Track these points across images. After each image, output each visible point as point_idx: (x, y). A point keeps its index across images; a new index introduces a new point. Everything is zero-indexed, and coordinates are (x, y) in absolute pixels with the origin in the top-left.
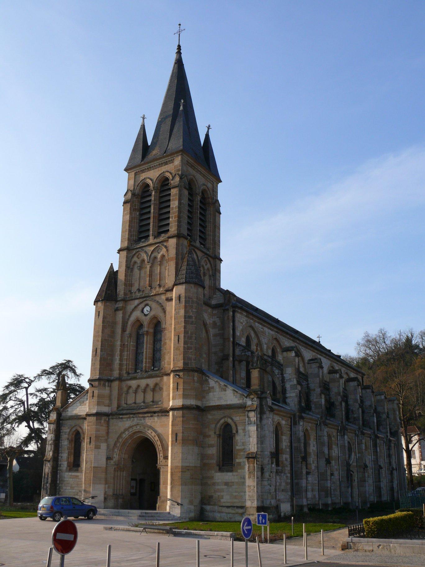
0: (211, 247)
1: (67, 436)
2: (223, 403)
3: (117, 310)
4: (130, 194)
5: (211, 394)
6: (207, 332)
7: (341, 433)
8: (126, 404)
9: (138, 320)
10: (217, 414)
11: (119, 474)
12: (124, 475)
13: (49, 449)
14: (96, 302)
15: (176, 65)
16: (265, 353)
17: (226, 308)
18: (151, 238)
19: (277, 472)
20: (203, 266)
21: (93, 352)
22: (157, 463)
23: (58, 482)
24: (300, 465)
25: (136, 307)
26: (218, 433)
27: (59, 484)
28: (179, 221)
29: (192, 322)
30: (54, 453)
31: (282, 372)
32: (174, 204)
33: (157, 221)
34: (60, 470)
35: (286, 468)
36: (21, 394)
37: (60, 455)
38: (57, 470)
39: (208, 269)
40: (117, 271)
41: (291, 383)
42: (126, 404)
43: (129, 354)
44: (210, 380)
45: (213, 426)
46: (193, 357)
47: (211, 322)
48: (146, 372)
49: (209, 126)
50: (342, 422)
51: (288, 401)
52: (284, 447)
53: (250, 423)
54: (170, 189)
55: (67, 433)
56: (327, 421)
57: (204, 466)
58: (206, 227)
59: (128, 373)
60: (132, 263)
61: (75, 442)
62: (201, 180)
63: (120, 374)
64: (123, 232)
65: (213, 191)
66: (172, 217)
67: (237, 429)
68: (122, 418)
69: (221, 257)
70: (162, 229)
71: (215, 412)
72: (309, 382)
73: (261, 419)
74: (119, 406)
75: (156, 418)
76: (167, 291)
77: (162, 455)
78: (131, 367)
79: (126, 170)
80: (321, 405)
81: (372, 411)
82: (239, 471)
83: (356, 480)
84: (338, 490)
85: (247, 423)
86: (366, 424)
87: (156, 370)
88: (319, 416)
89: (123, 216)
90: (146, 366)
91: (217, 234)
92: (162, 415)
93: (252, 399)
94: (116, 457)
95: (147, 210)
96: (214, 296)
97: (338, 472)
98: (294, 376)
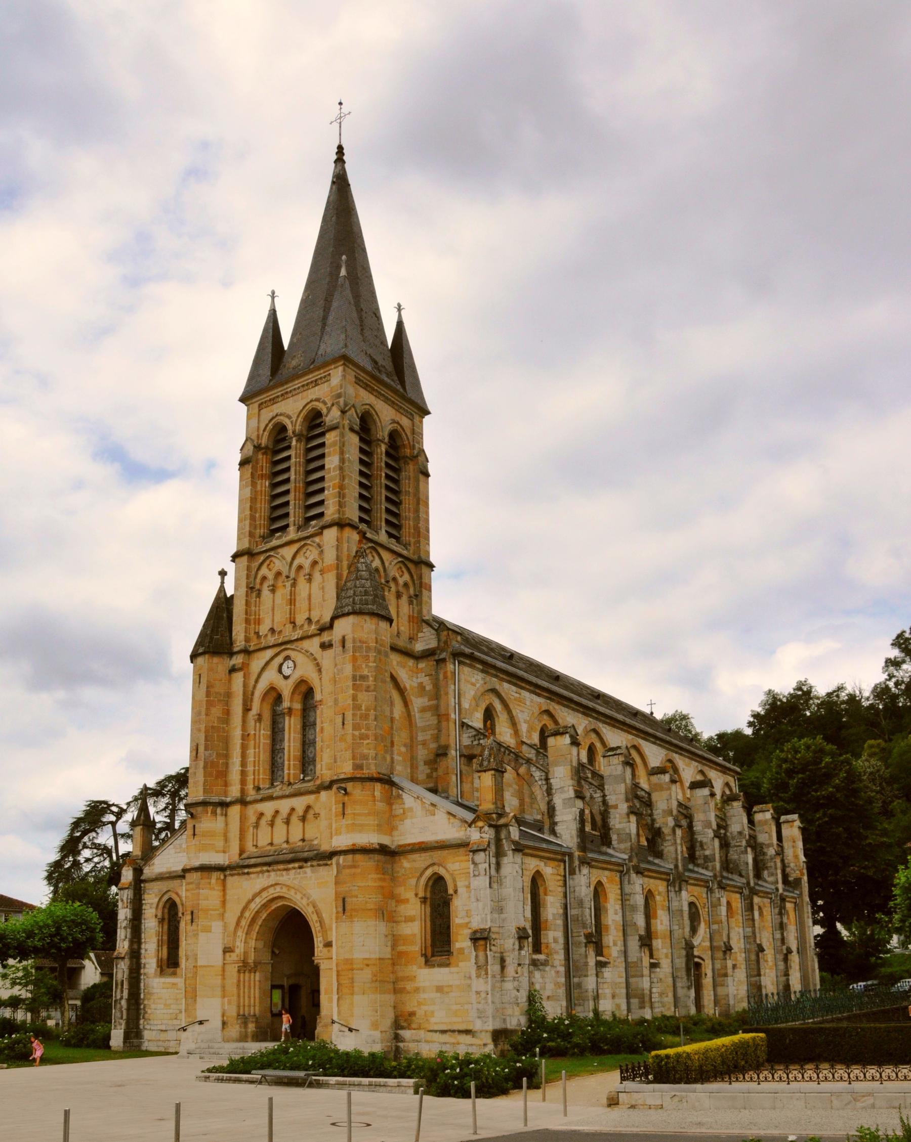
0: (412, 540)
1: (154, 910)
2: (429, 837)
3: (233, 670)
4: (250, 447)
5: (408, 822)
6: (406, 704)
7: (674, 887)
8: (256, 846)
9: (272, 689)
10: (420, 861)
11: (247, 979)
12: (257, 978)
13: (123, 937)
14: (194, 657)
15: (334, 187)
16: (525, 740)
17: (442, 656)
18: (292, 529)
19: (534, 963)
20: (394, 579)
21: (191, 752)
22: (313, 955)
23: (142, 996)
24: (584, 949)
25: (267, 663)
26: (421, 894)
27: (144, 1000)
28: (341, 495)
29: (368, 687)
30: (131, 942)
31: (547, 774)
32: (332, 462)
33: (302, 496)
34: (145, 974)
35: (555, 956)
36: (104, 837)
37: (143, 946)
38: (139, 974)
39: (406, 585)
40: (232, 596)
41: (566, 796)
42: (256, 846)
43: (259, 754)
44: (405, 796)
45: (413, 881)
46: (372, 753)
47: (416, 685)
48: (290, 784)
49: (399, 305)
50: (676, 866)
51: (558, 829)
52: (550, 917)
53: (476, 873)
54: (323, 434)
55: (155, 906)
56: (643, 866)
57: (397, 958)
58: (401, 503)
59: (258, 789)
60: (258, 580)
61: (169, 921)
62: (387, 416)
63: (243, 791)
64: (240, 520)
65: (413, 432)
66: (329, 487)
67: (455, 886)
68: (248, 873)
69: (433, 559)
70: (312, 514)
71: (416, 856)
72: (607, 793)
73: (498, 866)
74: (242, 851)
75: (308, 870)
76: (322, 629)
77: (320, 939)
78: (263, 776)
79: (243, 400)
80: (630, 835)
81: (744, 843)
82: (461, 964)
83: (710, 974)
84: (671, 994)
85: (472, 875)
86: (728, 865)
87: (309, 781)
88: (626, 857)
89: (240, 490)
90: (289, 774)
91: (422, 515)
92: (319, 865)
93: (481, 828)
94: (240, 948)
95: (285, 476)
96: (420, 635)
97: (669, 960)
98: (571, 782)
